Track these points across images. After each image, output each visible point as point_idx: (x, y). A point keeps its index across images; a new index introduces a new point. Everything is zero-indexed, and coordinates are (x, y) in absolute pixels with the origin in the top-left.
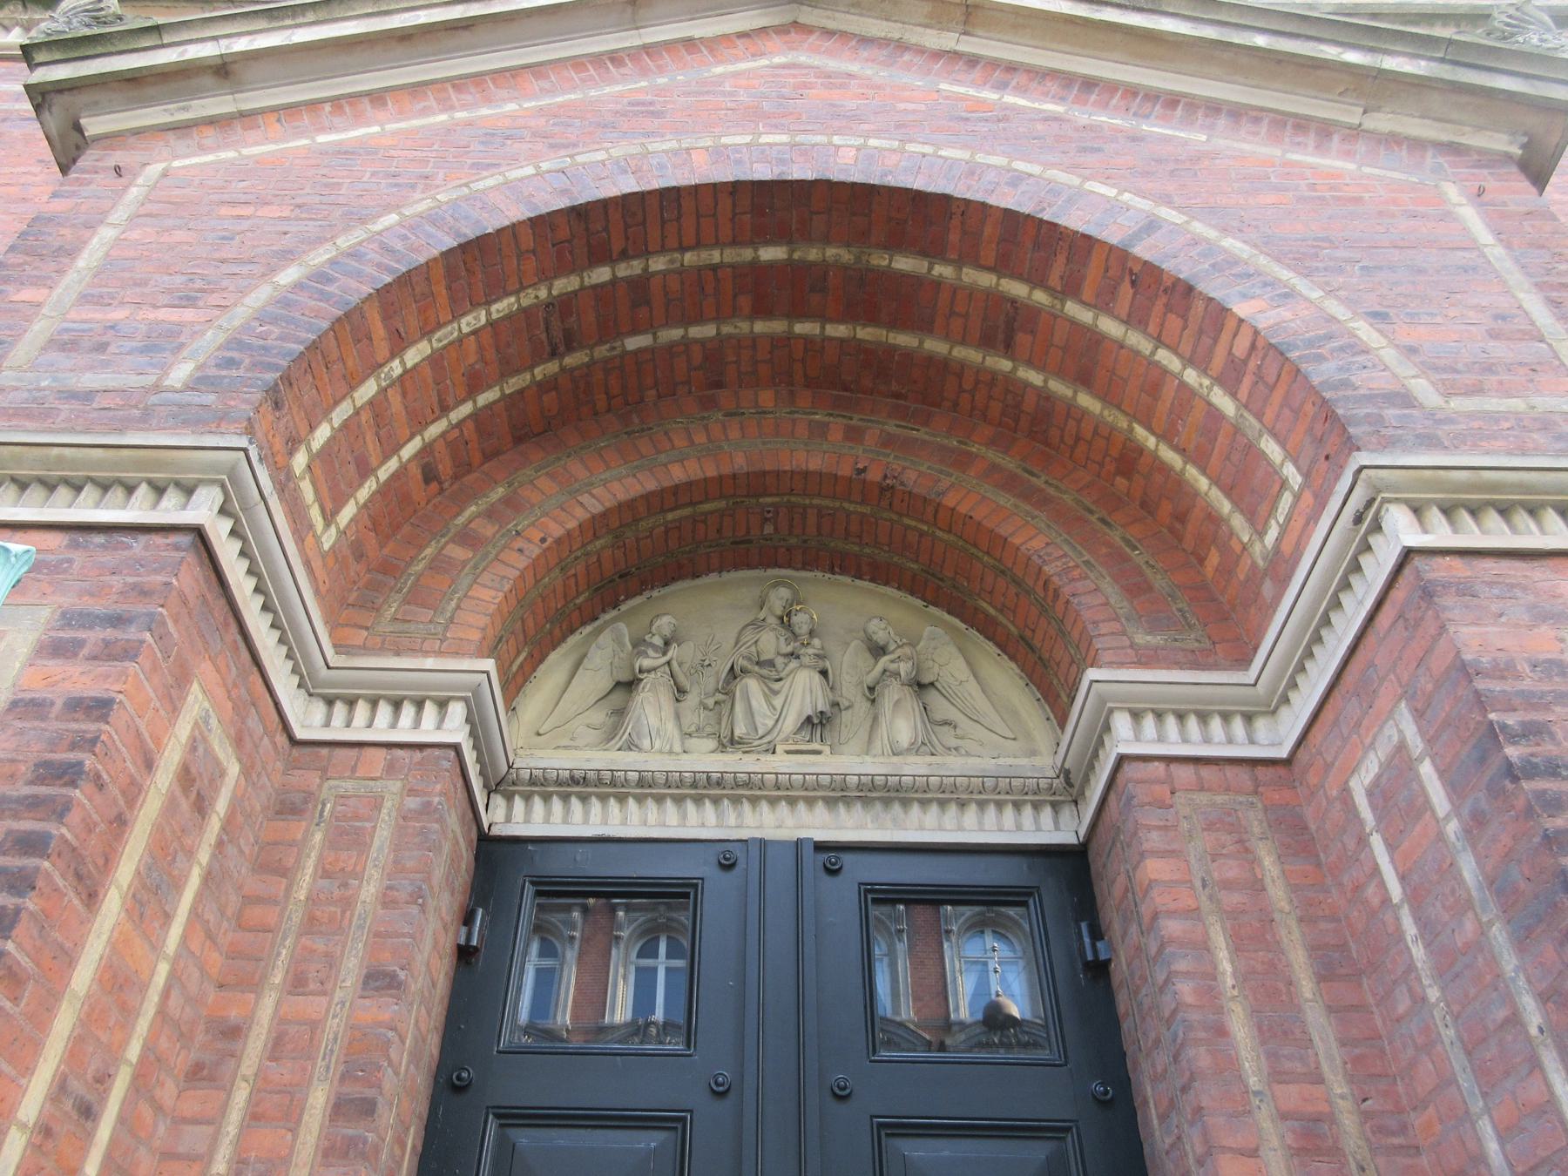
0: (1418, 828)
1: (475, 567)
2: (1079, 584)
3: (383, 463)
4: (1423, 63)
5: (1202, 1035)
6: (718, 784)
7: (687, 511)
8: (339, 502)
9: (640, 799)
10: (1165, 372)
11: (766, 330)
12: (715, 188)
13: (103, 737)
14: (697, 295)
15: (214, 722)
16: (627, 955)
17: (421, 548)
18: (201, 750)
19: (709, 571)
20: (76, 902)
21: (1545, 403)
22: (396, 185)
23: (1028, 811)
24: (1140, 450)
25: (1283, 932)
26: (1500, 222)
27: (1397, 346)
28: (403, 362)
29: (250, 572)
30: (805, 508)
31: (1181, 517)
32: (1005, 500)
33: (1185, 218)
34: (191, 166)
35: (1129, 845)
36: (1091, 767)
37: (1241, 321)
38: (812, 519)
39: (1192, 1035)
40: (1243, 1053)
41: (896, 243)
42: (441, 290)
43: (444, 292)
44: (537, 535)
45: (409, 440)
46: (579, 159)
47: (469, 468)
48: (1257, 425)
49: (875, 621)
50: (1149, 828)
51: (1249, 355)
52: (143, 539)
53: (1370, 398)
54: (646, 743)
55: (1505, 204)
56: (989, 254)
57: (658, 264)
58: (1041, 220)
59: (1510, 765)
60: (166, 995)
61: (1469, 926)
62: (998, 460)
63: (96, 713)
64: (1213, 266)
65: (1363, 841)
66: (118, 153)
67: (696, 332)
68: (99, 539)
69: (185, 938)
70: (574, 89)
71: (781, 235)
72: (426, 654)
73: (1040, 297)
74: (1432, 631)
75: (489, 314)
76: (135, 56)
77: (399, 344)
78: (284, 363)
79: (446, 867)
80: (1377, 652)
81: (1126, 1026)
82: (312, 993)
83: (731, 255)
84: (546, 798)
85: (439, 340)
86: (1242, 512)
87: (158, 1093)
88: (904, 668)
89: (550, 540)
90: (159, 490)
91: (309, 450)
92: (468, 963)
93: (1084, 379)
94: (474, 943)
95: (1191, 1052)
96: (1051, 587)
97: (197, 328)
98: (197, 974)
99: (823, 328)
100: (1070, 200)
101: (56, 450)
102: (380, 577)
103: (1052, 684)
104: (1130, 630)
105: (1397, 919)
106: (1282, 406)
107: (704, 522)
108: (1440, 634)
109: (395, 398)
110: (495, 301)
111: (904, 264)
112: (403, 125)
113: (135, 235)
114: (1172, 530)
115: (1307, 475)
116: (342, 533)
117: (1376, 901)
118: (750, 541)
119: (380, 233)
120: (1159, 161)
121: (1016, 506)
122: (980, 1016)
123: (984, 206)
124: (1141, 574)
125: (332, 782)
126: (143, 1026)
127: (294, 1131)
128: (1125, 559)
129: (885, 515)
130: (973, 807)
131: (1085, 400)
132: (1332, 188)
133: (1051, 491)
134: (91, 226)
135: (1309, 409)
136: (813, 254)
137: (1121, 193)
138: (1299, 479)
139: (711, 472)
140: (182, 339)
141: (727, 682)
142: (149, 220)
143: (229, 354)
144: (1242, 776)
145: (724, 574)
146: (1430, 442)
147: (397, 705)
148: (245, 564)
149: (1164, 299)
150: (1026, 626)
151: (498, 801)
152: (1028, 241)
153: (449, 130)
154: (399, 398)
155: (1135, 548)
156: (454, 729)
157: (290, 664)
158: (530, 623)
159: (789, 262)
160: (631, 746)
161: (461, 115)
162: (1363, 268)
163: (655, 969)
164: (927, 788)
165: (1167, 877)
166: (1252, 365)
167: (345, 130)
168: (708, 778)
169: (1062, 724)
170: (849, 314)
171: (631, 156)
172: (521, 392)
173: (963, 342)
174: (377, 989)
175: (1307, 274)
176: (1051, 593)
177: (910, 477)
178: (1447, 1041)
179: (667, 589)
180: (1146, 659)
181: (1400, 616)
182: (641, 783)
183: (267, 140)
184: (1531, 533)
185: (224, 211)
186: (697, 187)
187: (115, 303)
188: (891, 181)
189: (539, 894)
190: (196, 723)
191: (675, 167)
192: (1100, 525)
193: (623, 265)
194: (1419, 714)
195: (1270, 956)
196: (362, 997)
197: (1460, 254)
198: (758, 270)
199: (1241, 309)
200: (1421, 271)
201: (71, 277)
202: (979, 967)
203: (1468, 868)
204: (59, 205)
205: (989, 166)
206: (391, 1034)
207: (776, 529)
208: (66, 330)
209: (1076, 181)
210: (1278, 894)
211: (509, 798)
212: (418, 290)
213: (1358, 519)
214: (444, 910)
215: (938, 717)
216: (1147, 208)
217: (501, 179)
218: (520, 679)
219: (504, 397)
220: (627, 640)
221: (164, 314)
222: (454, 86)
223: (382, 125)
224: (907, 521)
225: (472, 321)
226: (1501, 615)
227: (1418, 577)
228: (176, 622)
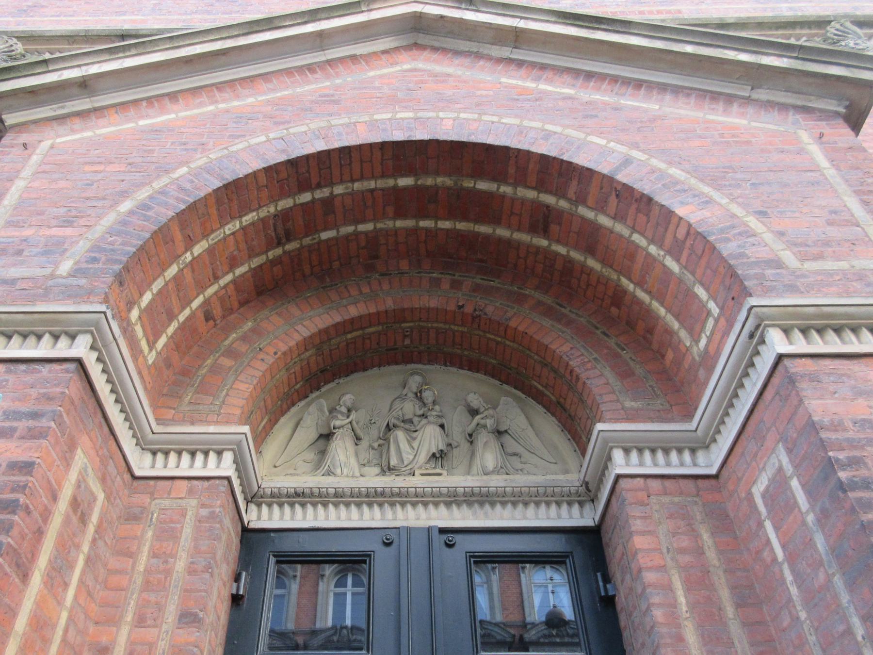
0: (791, 518)
1: (236, 371)
4: (785, 60)
5: (669, 641)
7: (359, 333)
8: (157, 337)
9: (336, 505)
10: (638, 246)
11: (402, 225)
12: (371, 146)
13: (30, 485)
14: (361, 207)
15: (90, 470)
16: (328, 585)
17: (205, 360)
18: (83, 486)
19: (373, 366)
20: (17, 580)
21: (860, 263)
22: (186, 150)
23: (565, 507)
24: (625, 292)
25: (716, 578)
26: (834, 155)
27: (773, 232)
28: (192, 254)
29: (108, 381)
32: (547, 323)
33: (647, 157)
34: (67, 142)
35: (624, 528)
37: (681, 218)
38: (432, 334)
39: (662, 641)
41: (478, 173)
42: (214, 211)
43: (215, 212)
44: (272, 350)
45: (196, 297)
46: (292, 131)
47: (231, 311)
49: (472, 395)
50: (635, 517)
51: (686, 238)
52: (48, 366)
53: (757, 263)
54: (339, 471)
55: (836, 143)
56: (532, 179)
57: (339, 190)
58: (562, 160)
60: (66, 631)
61: (822, 576)
62: (541, 298)
65: (760, 524)
66: (24, 135)
67: (362, 228)
68: (23, 367)
69: (76, 597)
70: (287, 88)
71: (410, 171)
72: (209, 423)
73: (563, 204)
74: (795, 402)
75: (241, 222)
76: (33, 78)
77: (190, 242)
78: (125, 259)
79: (225, 547)
80: (764, 414)
81: (626, 634)
82: (149, 627)
83: (382, 183)
84: (281, 505)
85: (213, 239)
86: (685, 328)
88: (489, 422)
89: (279, 353)
90: (56, 337)
91: (139, 307)
92: (238, 605)
93: (591, 250)
94: (241, 592)
96: (574, 374)
97: (74, 239)
98: (83, 617)
99: (436, 223)
100: (578, 148)
102: (181, 378)
104: (621, 399)
105: (781, 571)
107: (369, 338)
108: (800, 405)
109: (188, 274)
110: (245, 215)
111: (483, 185)
112: (188, 113)
113: (36, 184)
114: (645, 338)
115: (722, 308)
116: (159, 354)
117: (769, 560)
118: (397, 349)
119: (177, 179)
121: (553, 326)
122: (543, 619)
125: (157, 501)
128: (617, 356)
130: (532, 505)
131: (591, 263)
132: (733, 136)
133: (573, 316)
134: (11, 180)
136: (429, 181)
137: (608, 142)
138: (718, 311)
139: (373, 310)
140: (66, 246)
141: (385, 433)
143: (93, 255)
144: (690, 484)
145: (382, 368)
146: (792, 289)
147: (193, 454)
148: (105, 377)
150: (561, 396)
151: (253, 507)
152: (553, 172)
153: (215, 115)
154: (190, 274)
155: (623, 349)
156: (227, 467)
157: (131, 432)
158: (269, 402)
160: (329, 473)
161: (222, 106)
162: (752, 184)
163: (345, 594)
164: (505, 494)
165: (646, 546)
166: (688, 243)
168: (376, 491)
169: (583, 454)
170: (451, 215)
171: (322, 128)
172: (261, 266)
173: (519, 230)
174: (186, 623)
175: (719, 188)
177: (490, 310)
178: (812, 645)
179: (348, 378)
181: (777, 393)
182: (336, 495)
183: (110, 124)
184: (852, 343)
185: (87, 168)
186: (360, 146)
187: (26, 225)
188: (473, 139)
189: (278, 562)
190: (80, 472)
191: (347, 134)
192: (602, 336)
193: (318, 191)
194: (789, 451)
195: (708, 593)
196: (178, 628)
197: (809, 174)
198: (396, 190)
199: (680, 211)
200: (786, 185)
202: (543, 589)
203: (820, 541)
205: (531, 128)
206: (195, 650)
207: (411, 341)
209: (582, 136)
210: (711, 555)
211: (259, 505)
212: (200, 212)
213: (752, 336)
214: (223, 574)
216: (624, 151)
217: (246, 144)
218: (263, 434)
219: (251, 269)
220: (326, 409)
221: (55, 231)
222: (217, 88)
223: (176, 113)
224: (488, 335)
225: (233, 226)
226: (835, 393)
227: (787, 371)
228: (68, 414)
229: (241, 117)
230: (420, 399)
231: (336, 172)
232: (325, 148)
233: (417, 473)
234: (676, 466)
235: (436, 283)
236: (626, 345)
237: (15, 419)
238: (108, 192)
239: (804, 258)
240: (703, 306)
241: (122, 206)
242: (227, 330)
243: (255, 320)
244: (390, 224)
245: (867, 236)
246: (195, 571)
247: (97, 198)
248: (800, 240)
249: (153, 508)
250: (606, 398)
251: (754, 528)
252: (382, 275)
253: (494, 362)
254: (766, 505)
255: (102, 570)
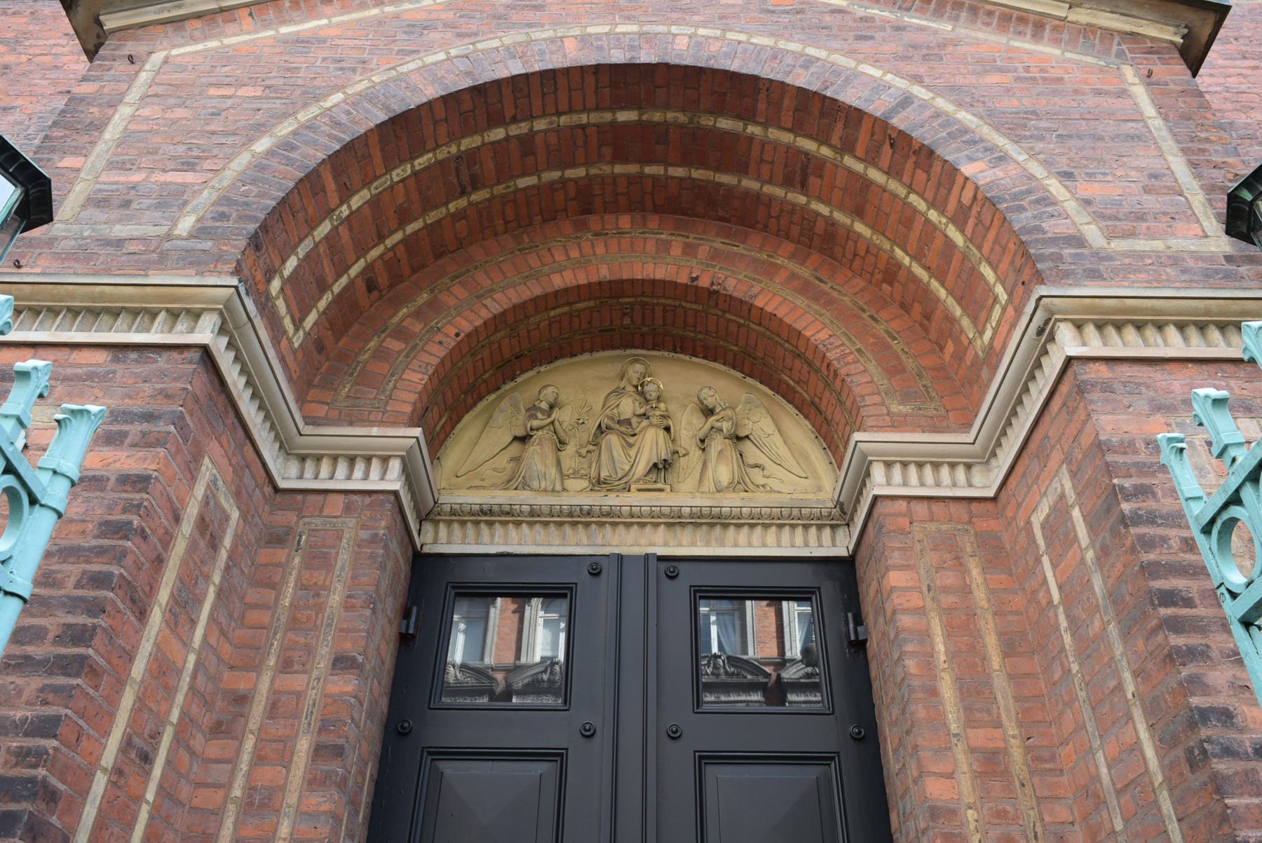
0: (1070, 554)
1: (407, 356)
2: (851, 367)
3: (336, 280)
6: (588, 514)
7: (566, 309)
8: (304, 314)
10: (915, 211)
11: (624, 171)
12: (582, 69)
13: (145, 503)
14: (566, 148)
15: (220, 483)
17: (367, 341)
18: (212, 503)
19: (583, 351)
20: (132, 618)
22: (342, 69)
24: (899, 265)
25: (983, 622)
28: (349, 207)
30: (653, 305)
31: (928, 316)
32: (801, 302)
33: (931, 95)
34: (185, 54)
36: (858, 501)
37: (967, 178)
38: (659, 312)
40: (948, 708)
41: (719, 110)
42: (377, 154)
46: (480, 46)
48: (979, 255)
51: (972, 204)
53: (1054, 241)
57: (540, 125)
58: (825, 97)
59: (1123, 516)
60: (194, 676)
61: (1097, 623)
63: (139, 486)
64: (949, 134)
65: (1038, 560)
67: (570, 173)
68: (133, 355)
69: (205, 636)
72: (372, 423)
73: (825, 151)
74: (1083, 417)
75: (413, 166)
77: (346, 193)
78: (262, 216)
81: (875, 686)
82: (296, 672)
83: (595, 118)
85: (376, 188)
87: (192, 742)
88: (726, 426)
91: (282, 276)
93: (859, 213)
94: (411, 631)
95: (912, 708)
97: (196, 188)
98: (215, 660)
99: (666, 170)
101: (98, 288)
103: (832, 438)
104: (887, 402)
106: (994, 243)
107: (578, 316)
109: (344, 232)
110: (417, 157)
111: (725, 124)
113: (146, 112)
114: (921, 325)
115: (1010, 295)
116: (307, 334)
119: (329, 109)
120: (915, 47)
123: (782, 84)
124: (898, 358)
125: (306, 520)
126: (180, 698)
127: (288, 768)
129: (713, 311)
130: (774, 528)
131: (860, 227)
132: (1042, 70)
133: (835, 294)
134: (113, 105)
135: (1011, 246)
136: (657, 117)
137: (884, 74)
138: (1005, 297)
139: (583, 280)
140: (185, 197)
142: (156, 100)
143: (221, 209)
146: (1094, 275)
149: (913, 159)
151: (428, 527)
152: (817, 111)
155: (895, 339)
156: (393, 481)
159: (639, 123)
162: (1058, 136)
167: (301, 22)
169: (840, 467)
170: (687, 160)
172: (439, 222)
173: (770, 182)
174: (342, 669)
175: (1017, 140)
176: (832, 373)
179: (552, 365)
180: (897, 424)
182: (532, 513)
184: (1157, 346)
185: (212, 91)
187: (134, 167)
190: (208, 485)
193: (514, 127)
194: (1073, 475)
197: (1130, 124)
199: (967, 169)
200: (1101, 138)
201: (100, 147)
203: (1098, 583)
204: (88, 88)
205: (788, 51)
208: (100, 190)
209: (851, 63)
212: (359, 153)
213: (1040, 332)
215: (751, 462)
216: (904, 86)
217: (420, 63)
224: (728, 316)
228: (191, 415)
229: (414, 26)
230: (642, 394)
231: (537, 103)
232: (523, 71)
233: (633, 487)
234: (947, 486)
235: (665, 247)
236: (898, 333)
237: (126, 422)
238: (240, 124)
239: (1110, 235)
240: (989, 290)
241: (258, 144)
242: (397, 303)
243: (432, 291)
244: (607, 169)
245: (1190, 208)
246: (353, 606)
247: (227, 134)
248: (1109, 211)
249: (301, 528)
250: (869, 400)
251: (1031, 563)
252: (597, 235)
253: (735, 348)
254: (1045, 537)
255: (238, 604)
